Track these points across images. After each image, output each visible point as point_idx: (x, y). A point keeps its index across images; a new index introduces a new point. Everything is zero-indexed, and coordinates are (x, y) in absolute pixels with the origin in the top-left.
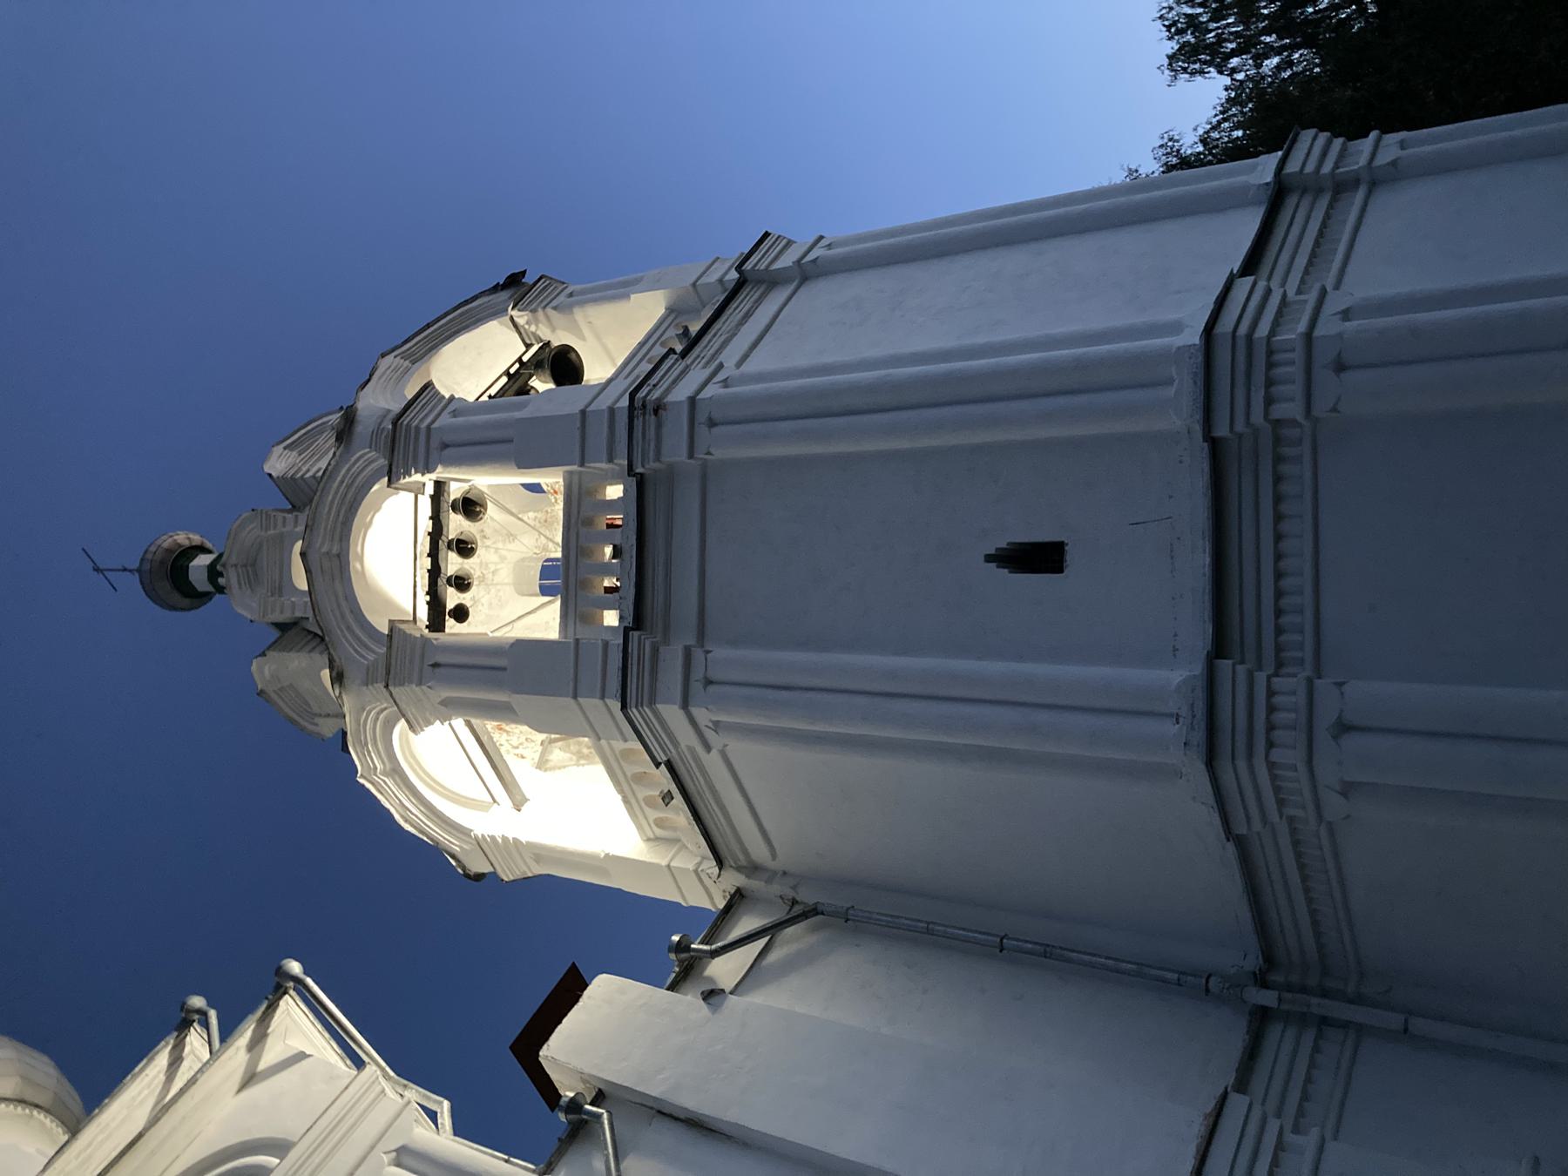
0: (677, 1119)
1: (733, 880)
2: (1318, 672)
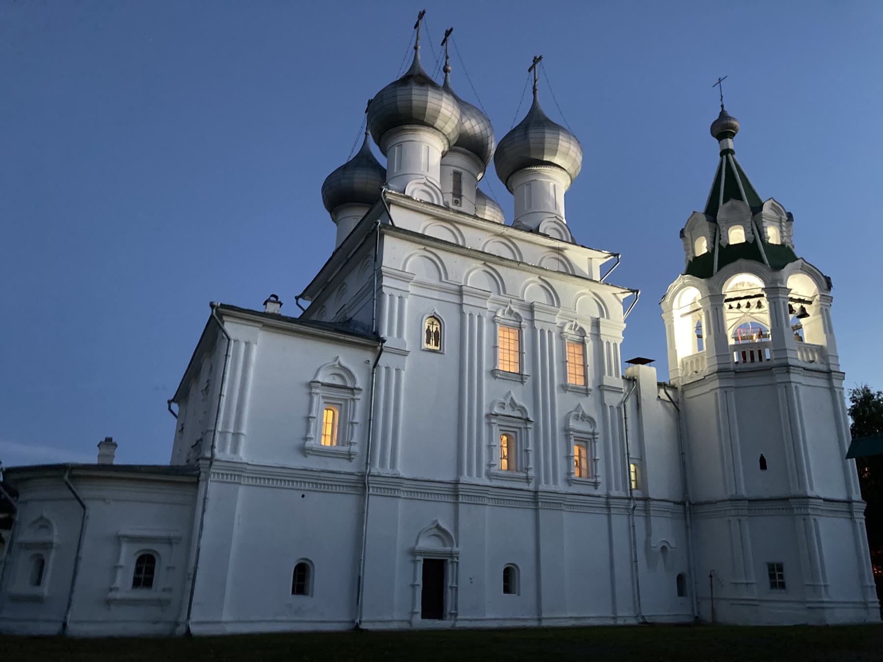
1: (680, 388)
2: (748, 516)
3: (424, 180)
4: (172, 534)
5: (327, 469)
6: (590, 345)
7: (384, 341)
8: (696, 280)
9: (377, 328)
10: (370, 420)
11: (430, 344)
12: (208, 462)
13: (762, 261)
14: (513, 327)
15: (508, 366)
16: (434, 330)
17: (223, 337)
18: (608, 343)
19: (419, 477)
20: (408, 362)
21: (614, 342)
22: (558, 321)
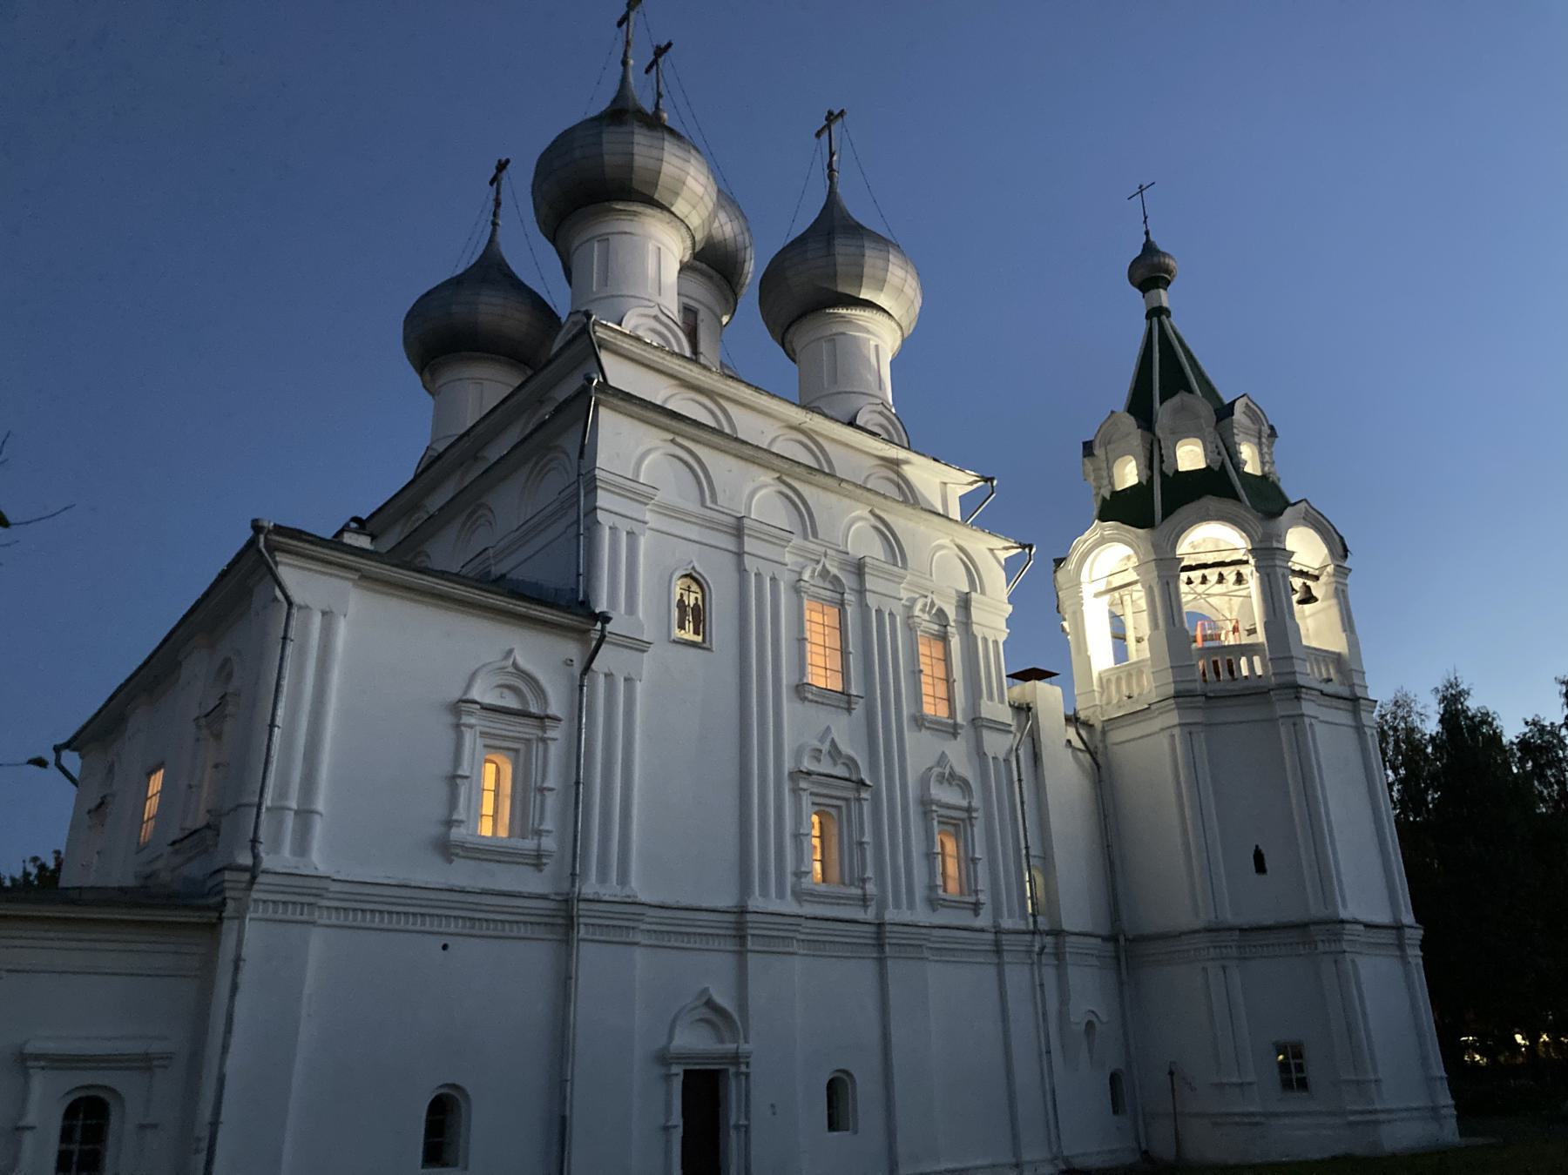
0: (1034, 747)
1: (1098, 726)
3: (655, 311)
4: (156, 1047)
5: (492, 887)
6: (955, 642)
7: (605, 619)
8: (1128, 531)
9: (586, 595)
10: (577, 783)
11: (685, 629)
12: (247, 876)
13: (1236, 497)
14: (831, 602)
15: (824, 679)
16: (692, 603)
17: (276, 599)
18: (985, 640)
19: (670, 901)
20: (647, 663)
21: (993, 638)
22: (904, 595)
